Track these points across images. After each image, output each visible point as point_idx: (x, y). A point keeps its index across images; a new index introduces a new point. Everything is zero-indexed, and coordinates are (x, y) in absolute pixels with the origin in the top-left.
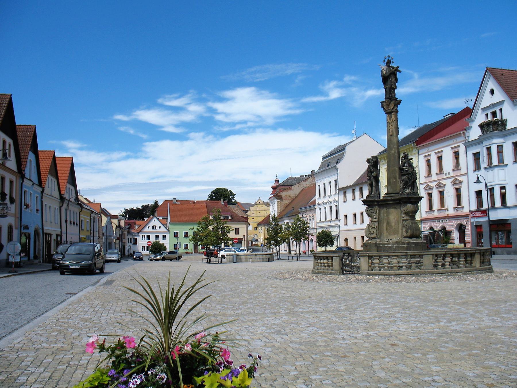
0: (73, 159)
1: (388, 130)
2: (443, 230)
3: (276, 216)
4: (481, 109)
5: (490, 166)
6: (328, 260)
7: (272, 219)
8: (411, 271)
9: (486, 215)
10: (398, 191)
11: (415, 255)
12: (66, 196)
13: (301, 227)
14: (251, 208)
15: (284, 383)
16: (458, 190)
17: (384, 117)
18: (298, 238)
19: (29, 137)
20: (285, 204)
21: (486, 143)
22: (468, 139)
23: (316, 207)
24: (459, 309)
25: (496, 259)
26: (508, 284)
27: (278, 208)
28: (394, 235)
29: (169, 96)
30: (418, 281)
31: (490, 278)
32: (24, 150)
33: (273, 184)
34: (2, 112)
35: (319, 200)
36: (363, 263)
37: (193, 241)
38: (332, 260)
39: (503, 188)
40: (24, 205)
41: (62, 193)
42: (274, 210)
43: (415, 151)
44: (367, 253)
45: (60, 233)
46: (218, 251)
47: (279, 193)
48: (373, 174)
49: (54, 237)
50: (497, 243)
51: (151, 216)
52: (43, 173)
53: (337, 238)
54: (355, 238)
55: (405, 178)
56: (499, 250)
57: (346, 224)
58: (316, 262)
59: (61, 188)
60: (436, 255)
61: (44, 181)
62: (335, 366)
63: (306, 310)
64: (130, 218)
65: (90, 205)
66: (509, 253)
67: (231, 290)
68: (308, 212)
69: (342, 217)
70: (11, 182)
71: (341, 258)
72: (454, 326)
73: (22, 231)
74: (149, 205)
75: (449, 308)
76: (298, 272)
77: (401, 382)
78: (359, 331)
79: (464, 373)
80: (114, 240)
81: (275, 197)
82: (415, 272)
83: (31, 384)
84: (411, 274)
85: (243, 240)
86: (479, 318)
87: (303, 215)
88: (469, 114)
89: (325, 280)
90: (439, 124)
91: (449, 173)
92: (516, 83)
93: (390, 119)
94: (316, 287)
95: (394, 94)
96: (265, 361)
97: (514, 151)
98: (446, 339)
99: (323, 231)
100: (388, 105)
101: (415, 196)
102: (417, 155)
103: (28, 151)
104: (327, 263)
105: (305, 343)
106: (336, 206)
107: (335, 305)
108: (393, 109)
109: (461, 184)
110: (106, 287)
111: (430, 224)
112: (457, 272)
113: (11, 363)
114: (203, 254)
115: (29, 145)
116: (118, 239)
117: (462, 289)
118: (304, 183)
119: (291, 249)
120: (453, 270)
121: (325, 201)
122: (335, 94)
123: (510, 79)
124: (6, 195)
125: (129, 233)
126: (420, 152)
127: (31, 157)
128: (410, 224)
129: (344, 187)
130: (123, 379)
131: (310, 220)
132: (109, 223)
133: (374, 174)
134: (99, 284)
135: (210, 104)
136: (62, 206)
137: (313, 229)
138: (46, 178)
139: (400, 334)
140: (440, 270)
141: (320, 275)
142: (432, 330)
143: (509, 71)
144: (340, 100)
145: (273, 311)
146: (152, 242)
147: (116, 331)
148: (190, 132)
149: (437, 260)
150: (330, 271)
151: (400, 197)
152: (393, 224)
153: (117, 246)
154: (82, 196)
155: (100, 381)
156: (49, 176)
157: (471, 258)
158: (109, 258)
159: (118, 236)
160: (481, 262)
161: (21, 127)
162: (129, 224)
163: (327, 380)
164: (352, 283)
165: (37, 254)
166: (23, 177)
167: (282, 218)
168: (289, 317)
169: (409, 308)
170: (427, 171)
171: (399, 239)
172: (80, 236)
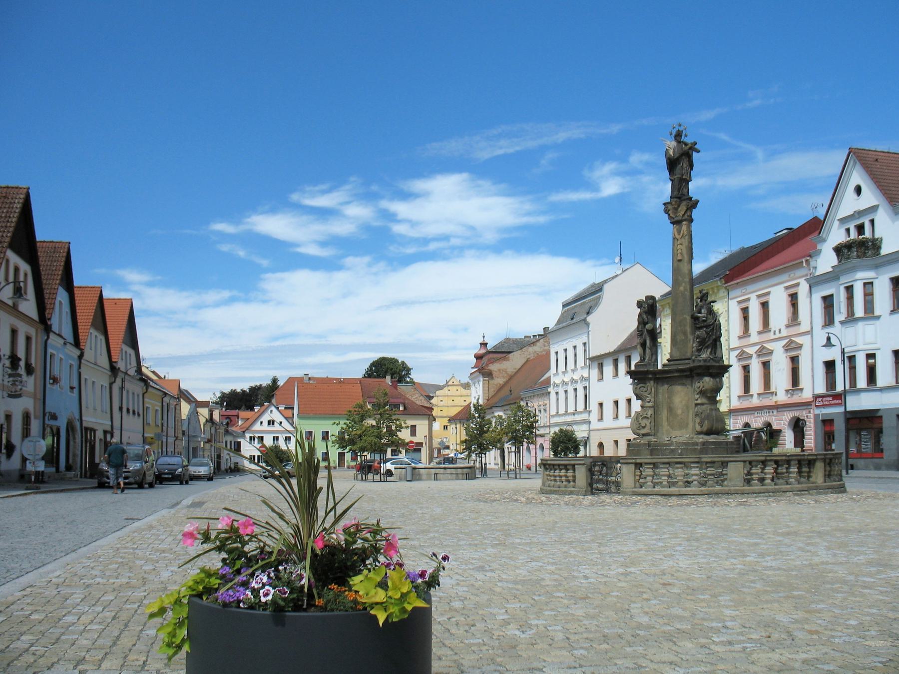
0: (132, 303)
1: (675, 250)
2: (766, 428)
3: (481, 402)
4: (838, 220)
5: (851, 318)
6: (567, 470)
7: (474, 407)
8: (707, 488)
9: (840, 402)
10: (689, 355)
11: (714, 462)
12: (121, 365)
13: (523, 421)
14: (438, 393)
15: (486, 628)
16: (794, 360)
18: (517, 441)
19: (58, 261)
20: (496, 385)
21: (845, 280)
22: (814, 271)
23: (549, 390)
24: (779, 541)
25: (856, 477)
26: (867, 509)
27: (484, 392)
28: (681, 429)
30: (718, 505)
31: (839, 500)
32: (49, 284)
33: (477, 350)
34: (14, 217)
35: (556, 376)
36: (627, 475)
38: (574, 470)
39: (870, 356)
40: (50, 379)
41: (113, 360)
42: (477, 394)
43: (723, 293)
44: (633, 459)
45: (109, 429)
46: (379, 463)
47: (487, 365)
48: (647, 326)
49: (100, 435)
50: (857, 450)
51: (266, 404)
52: (81, 324)
53: (586, 444)
54: (616, 442)
55: (701, 333)
56: (861, 462)
57: (601, 419)
58: (547, 475)
59: (112, 352)
60: (750, 463)
61: (83, 338)
62: (569, 610)
63: (527, 541)
64: (228, 407)
65: (159, 382)
66: (878, 468)
67: (403, 515)
68: (536, 399)
69: (594, 407)
70: (28, 339)
72: (769, 562)
73: (47, 422)
74: (261, 385)
75: (764, 539)
76: (516, 491)
77: (672, 628)
78: (612, 568)
79: (774, 619)
80: (202, 443)
81: (480, 373)
82: (713, 490)
83: (85, 625)
84: (707, 493)
85: (424, 445)
86: (811, 552)
87: (527, 404)
88: (818, 229)
89: (562, 502)
90: (765, 247)
91: (780, 330)
92: (898, 172)
93: (679, 232)
94: (546, 512)
95: (686, 190)
96: (457, 603)
97: (892, 292)
98: (752, 578)
99: (561, 431)
100: (676, 209)
101: (718, 364)
102: (726, 300)
103: (57, 286)
104: (566, 476)
105: (523, 582)
106: (585, 388)
107: (575, 534)
108: (683, 215)
110: (192, 509)
112: (785, 490)
113: (49, 601)
114: (355, 469)
115: (58, 275)
117: (789, 515)
119: (506, 462)
120: (777, 487)
121: (566, 380)
122: (611, 188)
123: (890, 168)
124: (20, 359)
125: (227, 432)
126: (732, 294)
127: (62, 296)
128: (708, 411)
129: (599, 354)
130: (241, 579)
131: (540, 411)
132: (194, 414)
133: (649, 326)
134: (179, 507)
135: (385, 204)
136: (115, 382)
137: (544, 426)
138: (87, 334)
139: (678, 571)
141: (554, 496)
142: (732, 567)
143: (889, 155)
144: (620, 198)
145: (472, 542)
147: (213, 564)
148: (347, 256)
149: (752, 471)
150: (570, 489)
151: (692, 365)
152: (679, 412)
153: (207, 453)
154: (148, 368)
155: (207, 584)
156: (92, 331)
157: (809, 468)
158: (193, 472)
159: (209, 438)
160: (825, 475)
161: (45, 244)
162: (228, 417)
163: (555, 625)
164: (606, 507)
165: (71, 461)
166: (48, 329)
167: (491, 408)
168: (499, 550)
169: (697, 540)
170: (743, 327)
171: (688, 436)
172: (143, 436)
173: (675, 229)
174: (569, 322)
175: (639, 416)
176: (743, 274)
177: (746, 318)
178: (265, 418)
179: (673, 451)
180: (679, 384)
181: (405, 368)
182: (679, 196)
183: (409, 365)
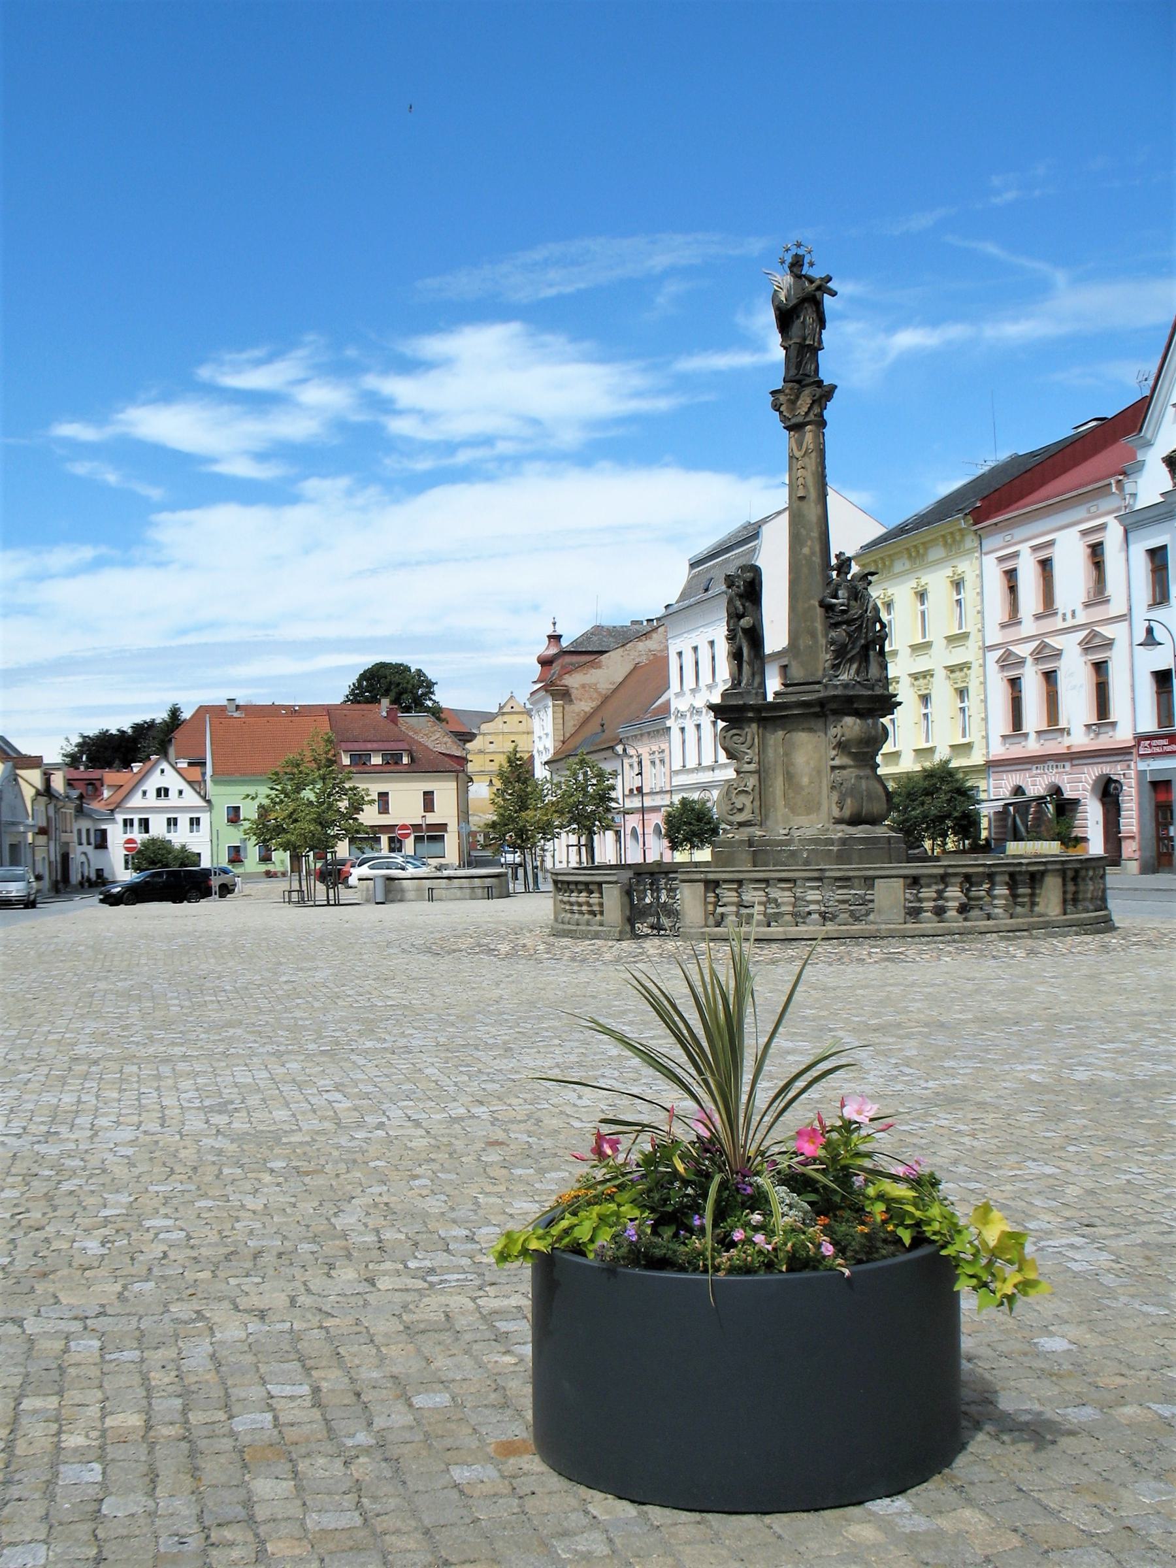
1: (794, 480)
8: (837, 927)
11: (848, 879)
16: (1100, 668)
17: (782, 440)
23: (669, 723)
28: (808, 814)
29: (235, 356)
33: (542, 648)
37: (255, 834)
47: (560, 676)
55: (839, 634)
71: (627, 888)
81: (547, 691)
91: (1074, 612)
93: (800, 444)
95: (813, 367)
99: (684, 802)
100: (793, 403)
102: (976, 555)
108: (807, 413)
109: (1111, 649)
111: (1011, 780)
116: (43, 831)
118: (642, 646)
125: (80, 811)
126: (988, 544)
128: (853, 781)
133: (745, 622)
135: (372, 382)
140: (929, 925)
146: (139, 842)
148: (306, 477)
149: (946, 894)
152: (805, 781)
157: (1033, 888)
160: (1065, 901)
173: (793, 439)
174: (701, 596)
175: (732, 788)
176: (1008, 506)
177: (1013, 589)
178: (154, 782)
179: (793, 854)
180: (803, 730)
181: (423, 681)
182: (798, 377)
183: (431, 675)
